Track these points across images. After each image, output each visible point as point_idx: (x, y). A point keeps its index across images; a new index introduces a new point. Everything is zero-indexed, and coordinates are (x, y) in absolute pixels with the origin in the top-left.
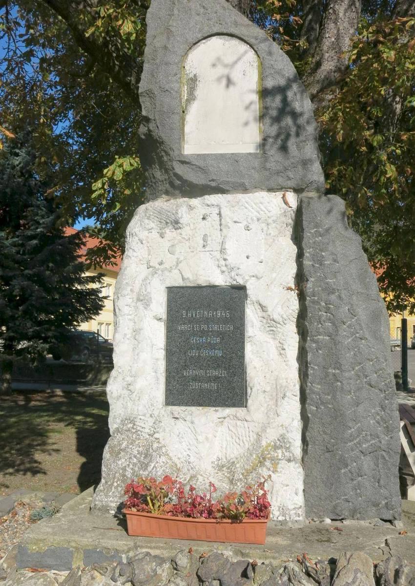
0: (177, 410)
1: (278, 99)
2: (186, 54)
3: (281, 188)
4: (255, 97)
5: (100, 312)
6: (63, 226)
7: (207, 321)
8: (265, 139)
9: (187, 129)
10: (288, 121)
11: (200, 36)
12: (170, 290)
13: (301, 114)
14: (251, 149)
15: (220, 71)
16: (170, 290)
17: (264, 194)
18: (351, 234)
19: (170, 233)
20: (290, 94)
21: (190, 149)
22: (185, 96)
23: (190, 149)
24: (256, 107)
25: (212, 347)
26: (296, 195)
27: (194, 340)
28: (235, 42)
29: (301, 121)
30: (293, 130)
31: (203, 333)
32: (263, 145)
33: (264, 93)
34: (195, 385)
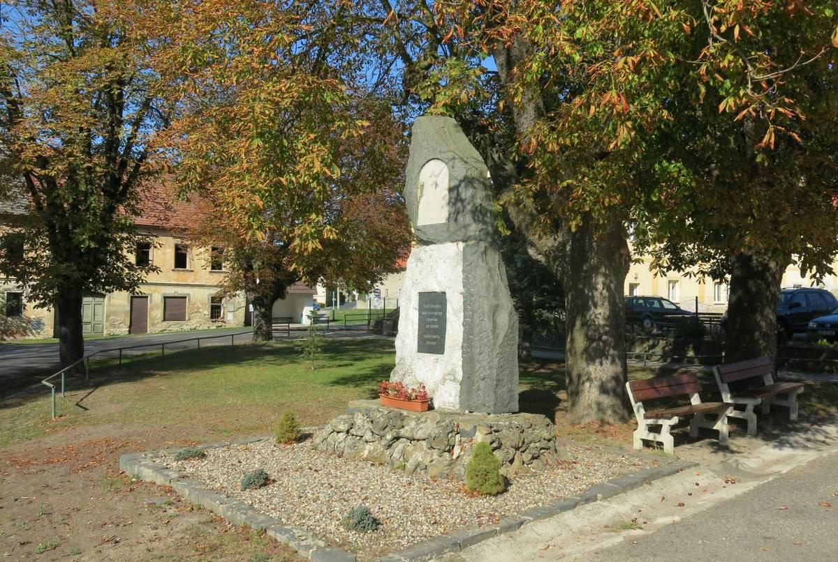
0: (421, 355)
1: (456, 192)
2: (420, 172)
3: (456, 241)
4: (447, 192)
5: (652, 482)
6: (803, 251)
7: (433, 310)
8: (450, 215)
9: (419, 212)
10: (459, 204)
11: (425, 161)
12: (420, 293)
13: (465, 199)
14: (444, 221)
15: (433, 179)
16: (420, 293)
17: (450, 244)
18: (411, 263)
19: (419, 264)
20: (460, 189)
21: (420, 223)
22: (419, 195)
23: (420, 223)
24: (447, 197)
25: (434, 323)
26: (416, 251)
27: (428, 320)
28: (440, 162)
29: (465, 203)
30: (461, 208)
31: (431, 316)
32: (449, 219)
33: (450, 190)
34: (428, 343)
